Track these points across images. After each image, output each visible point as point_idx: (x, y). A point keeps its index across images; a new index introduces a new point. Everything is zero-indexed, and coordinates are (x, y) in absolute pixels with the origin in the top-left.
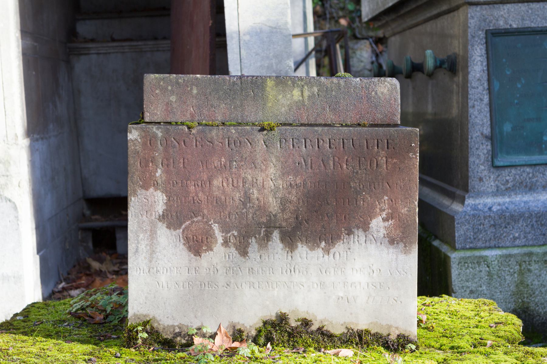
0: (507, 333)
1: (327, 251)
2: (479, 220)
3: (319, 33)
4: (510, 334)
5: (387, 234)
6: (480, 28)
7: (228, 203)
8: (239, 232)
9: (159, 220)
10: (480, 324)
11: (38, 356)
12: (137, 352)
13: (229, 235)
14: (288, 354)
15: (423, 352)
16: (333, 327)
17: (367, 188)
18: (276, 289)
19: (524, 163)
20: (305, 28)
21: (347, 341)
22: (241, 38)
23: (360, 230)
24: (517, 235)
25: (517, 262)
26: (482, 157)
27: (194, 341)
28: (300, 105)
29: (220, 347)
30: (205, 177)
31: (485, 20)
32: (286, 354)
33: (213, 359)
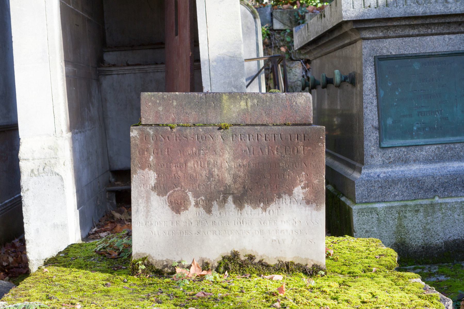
0: (387, 262)
1: (264, 209)
2: (371, 183)
3: (267, 57)
4: (388, 262)
5: (305, 197)
6: (370, 55)
7: (198, 178)
8: (206, 197)
10: (369, 256)
11: (72, 282)
12: (138, 279)
13: (199, 199)
14: (239, 279)
15: (330, 276)
16: (269, 260)
17: (291, 167)
18: (231, 235)
19: (401, 145)
20: (258, 54)
21: (279, 270)
22: (210, 64)
23: (287, 195)
24: (397, 193)
25: (397, 211)
26: (373, 141)
27: (176, 270)
28: (246, 112)
29: (193, 275)
30: (182, 161)
31: (373, 50)
32: (238, 279)
33: (188, 283)
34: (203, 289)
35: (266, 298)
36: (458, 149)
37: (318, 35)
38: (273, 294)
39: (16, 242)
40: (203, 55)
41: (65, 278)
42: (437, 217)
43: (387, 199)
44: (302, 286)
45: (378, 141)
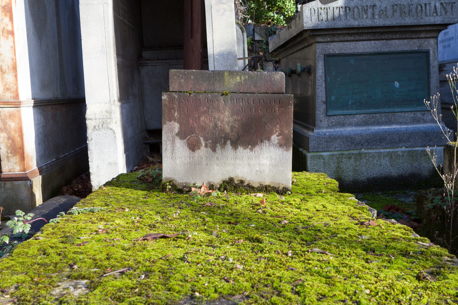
1: (251, 150)
3: (250, 58)
8: (212, 141)
9: (176, 135)
11: (122, 196)
12: (166, 194)
19: (340, 114)
23: (267, 140)
24: (337, 146)
26: (322, 111)
28: (240, 84)
29: (204, 192)
30: (197, 116)
31: (324, 50)
33: (200, 197)
34: (210, 201)
35: (253, 207)
36: (378, 118)
37: (286, 40)
38: (257, 205)
39: (84, 176)
40: (210, 51)
41: (117, 193)
42: (363, 162)
43: (330, 150)
44: (276, 201)
45: (325, 112)
